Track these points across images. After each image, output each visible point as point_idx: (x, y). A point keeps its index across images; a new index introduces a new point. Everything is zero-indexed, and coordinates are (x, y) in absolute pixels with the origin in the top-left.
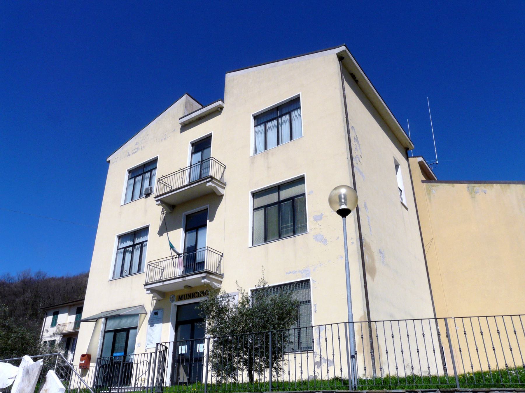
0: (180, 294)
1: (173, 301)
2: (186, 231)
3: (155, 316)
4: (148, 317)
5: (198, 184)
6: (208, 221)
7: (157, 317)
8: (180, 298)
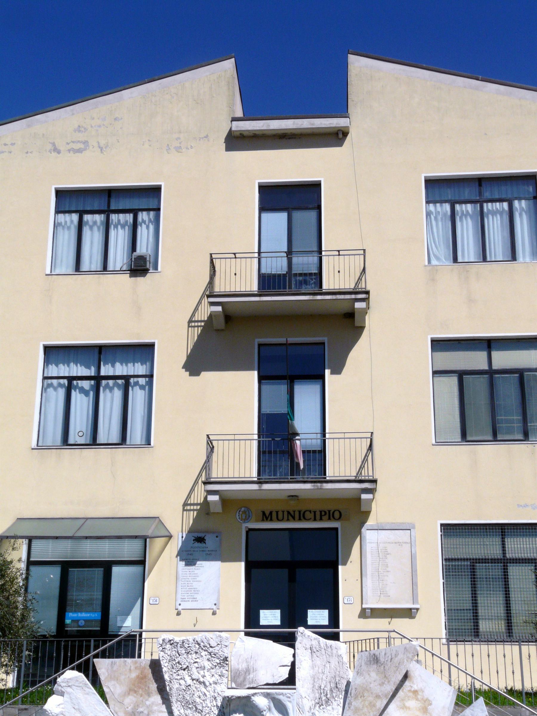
0: (267, 509)
1: (247, 519)
2: (261, 379)
3: (197, 544)
4: (176, 544)
5: (334, 297)
6: (327, 372)
7: (198, 545)
8: (266, 517)
